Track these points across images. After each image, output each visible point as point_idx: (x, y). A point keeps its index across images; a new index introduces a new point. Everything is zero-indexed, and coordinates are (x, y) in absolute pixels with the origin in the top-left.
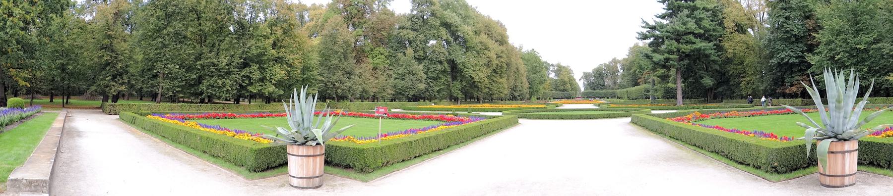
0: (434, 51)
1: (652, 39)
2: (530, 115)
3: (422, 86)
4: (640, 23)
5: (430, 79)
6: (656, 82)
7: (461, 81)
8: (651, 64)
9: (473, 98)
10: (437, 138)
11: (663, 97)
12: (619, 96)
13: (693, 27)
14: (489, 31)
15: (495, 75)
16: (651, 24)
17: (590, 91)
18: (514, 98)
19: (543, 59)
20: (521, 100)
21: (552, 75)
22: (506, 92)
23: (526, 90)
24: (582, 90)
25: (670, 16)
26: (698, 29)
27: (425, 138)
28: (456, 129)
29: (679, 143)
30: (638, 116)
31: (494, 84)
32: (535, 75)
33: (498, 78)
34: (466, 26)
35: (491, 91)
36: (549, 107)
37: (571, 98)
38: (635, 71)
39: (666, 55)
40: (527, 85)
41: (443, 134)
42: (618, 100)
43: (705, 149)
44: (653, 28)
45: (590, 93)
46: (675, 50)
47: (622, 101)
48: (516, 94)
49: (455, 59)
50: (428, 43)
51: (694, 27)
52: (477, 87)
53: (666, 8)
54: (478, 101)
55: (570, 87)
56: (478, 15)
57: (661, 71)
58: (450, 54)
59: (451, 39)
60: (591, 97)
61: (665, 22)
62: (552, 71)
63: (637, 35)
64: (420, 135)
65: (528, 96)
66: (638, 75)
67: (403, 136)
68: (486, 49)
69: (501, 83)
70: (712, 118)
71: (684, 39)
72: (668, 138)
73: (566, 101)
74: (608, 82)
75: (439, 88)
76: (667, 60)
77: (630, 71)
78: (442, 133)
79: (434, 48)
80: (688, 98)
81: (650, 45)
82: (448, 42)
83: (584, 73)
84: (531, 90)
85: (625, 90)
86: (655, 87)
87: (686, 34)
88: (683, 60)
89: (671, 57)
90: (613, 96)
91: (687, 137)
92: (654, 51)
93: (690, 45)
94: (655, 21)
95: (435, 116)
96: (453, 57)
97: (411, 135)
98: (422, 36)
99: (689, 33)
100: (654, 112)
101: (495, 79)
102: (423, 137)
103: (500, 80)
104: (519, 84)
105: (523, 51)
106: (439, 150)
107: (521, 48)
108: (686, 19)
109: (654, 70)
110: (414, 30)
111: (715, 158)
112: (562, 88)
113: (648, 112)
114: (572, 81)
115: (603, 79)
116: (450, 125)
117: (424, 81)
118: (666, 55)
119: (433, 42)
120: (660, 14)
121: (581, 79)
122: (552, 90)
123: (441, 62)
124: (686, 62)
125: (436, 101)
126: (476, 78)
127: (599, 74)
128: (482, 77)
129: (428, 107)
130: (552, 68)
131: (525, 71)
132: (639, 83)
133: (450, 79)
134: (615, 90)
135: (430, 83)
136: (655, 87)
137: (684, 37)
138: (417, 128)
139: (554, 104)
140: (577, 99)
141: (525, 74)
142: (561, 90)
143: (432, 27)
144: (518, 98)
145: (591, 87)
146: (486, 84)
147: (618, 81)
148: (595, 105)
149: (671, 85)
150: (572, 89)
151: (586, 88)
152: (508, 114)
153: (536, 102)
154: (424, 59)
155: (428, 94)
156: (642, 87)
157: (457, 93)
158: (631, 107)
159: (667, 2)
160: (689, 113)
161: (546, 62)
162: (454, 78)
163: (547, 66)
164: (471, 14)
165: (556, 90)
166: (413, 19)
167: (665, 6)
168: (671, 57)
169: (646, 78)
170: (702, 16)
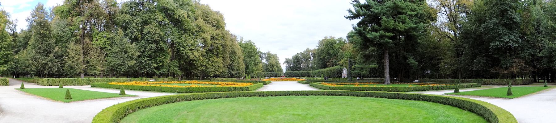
17: (291, 71)
31: (210, 63)
33: (215, 58)
35: (208, 69)
37: (277, 77)
38: (324, 57)
40: (244, 66)
45: (290, 73)
48: (234, 73)
55: (276, 69)
66: (327, 59)
69: (217, 62)
73: (274, 79)
83: (286, 59)
89: (387, 34)
101: (211, 59)
103: (216, 60)
112: (271, 69)
114: (277, 64)
115: (299, 63)
121: (284, 64)
122: (263, 71)
126: (192, 57)
127: (297, 60)
132: (328, 66)
134: (309, 71)
140: (282, 77)
141: (242, 58)
142: (270, 71)
144: (236, 76)
145: (291, 69)
150: (278, 70)
151: (288, 70)
163: (261, 54)
165: (267, 71)
168: (387, 34)
169: (333, 62)
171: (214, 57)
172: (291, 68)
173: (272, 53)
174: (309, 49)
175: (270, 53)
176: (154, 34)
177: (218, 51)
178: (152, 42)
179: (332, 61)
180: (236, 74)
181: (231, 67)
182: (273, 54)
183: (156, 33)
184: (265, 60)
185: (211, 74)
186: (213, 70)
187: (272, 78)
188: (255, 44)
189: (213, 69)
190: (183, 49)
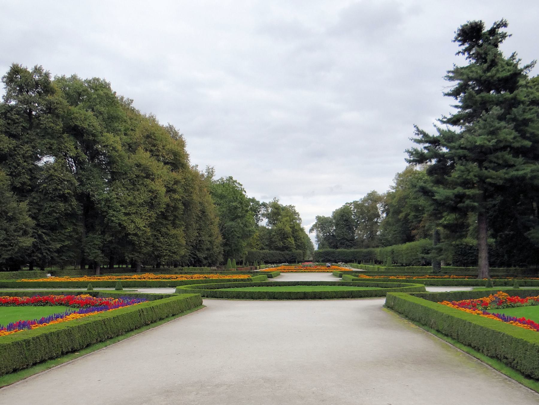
0: (50, 178)
1: (434, 162)
2: (223, 292)
3: (28, 242)
4: (411, 133)
5: (43, 227)
6: (442, 236)
7: (103, 233)
8: (431, 205)
9: (123, 262)
10: (69, 332)
11: (456, 262)
12: (379, 259)
13: (510, 138)
14: (154, 146)
15: (164, 222)
16: (431, 135)
18: (196, 262)
19: (249, 195)
20: (210, 265)
21: (264, 222)
22: (183, 252)
23: (218, 249)
24: (316, 247)
25: (468, 118)
26: (519, 139)
27: (51, 334)
28: (100, 319)
29: (446, 342)
30: (395, 297)
31: (162, 239)
32: (233, 223)
34: (110, 135)
35: (157, 250)
36: (256, 279)
37: (295, 262)
38: (407, 215)
39: (459, 190)
40: (220, 240)
41: (79, 327)
42: (376, 266)
43: (483, 352)
44: (435, 142)
46: (476, 180)
47: (382, 268)
48: (201, 255)
49: (91, 193)
50: (39, 160)
51: (512, 136)
52: (132, 243)
53: (460, 104)
54: (134, 269)
55: (293, 242)
56: (134, 114)
57: (449, 218)
58: (82, 183)
59: (85, 157)
60: (329, 261)
61: (457, 130)
62: (263, 215)
63: (407, 156)
64: (38, 330)
65: (221, 258)
67: (7, 333)
68: (148, 176)
69: (175, 236)
70: (532, 305)
71: (491, 162)
72: (434, 332)
73: (287, 268)
74: (359, 234)
75: (59, 245)
76: (460, 197)
77: (398, 215)
78: (77, 325)
79: (52, 171)
80: (501, 265)
81: (431, 171)
82: (79, 163)
83: (319, 218)
84: (228, 248)
85: (389, 248)
86: (439, 245)
87: (495, 149)
88: (491, 196)
89: (468, 192)
90: (369, 258)
91: (460, 332)
92: (438, 182)
93: (504, 170)
94: (439, 130)
95: (57, 297)
96: (88, 189)
97: (22, 330)
98: (26, 147)
99: (504, 148)
100: (430, 290)
101: (164, 230)
102: (47, 332)
103: (173, 232)
104: (205, 238)
105: (215, 178)
106: (74, 351)
107: (211, 173)
108: (497, 124)
109: (436, 215)
110: (11, 135)
111: (495, 366)
113: (419, 290)
116: (86, 312)
117: (31, 231)
118: (459, 190)
119: (48, 160)
120: (449, 117)
122: (262, 249)
123: (64, 198)
124: (499, 199)
125: (54, 269)
128: (141, 225)
129: (41, 280)
130: (263, 211)
131: (216, 217)
133: (81, 229)
135: (44, 236)
136: (439, 245)
137: (492, 157)
138: (31, 319)
139: (264, 273)
140: (306, 264)
142: (277, 249)
143: (46, 133)
144: (205, 262)
145: (330, 243)
146: (149, 239)
147: (378, 233)
148: (335, 275)
149: (470, 240)
151: (321, 246)
152: (186, 292)
153: (234, 270)
154: (31, 191)
155: (40, 255)
156: (420, 243)
157: (94, 255)
158: (394, 281)
159: (462, 94)
160: (487, 294)
161: (253, 200)
162: (90, 228)
164: (121, 112)
165: (271, 248)
166: (9, 115)
167: (457, 102)
168: (468, 192)
170: (528, 116)
171: (168, 226)
172: (331, 241)
173: (284, 202)
174: (376, 192)
175: (279, 203)
176: (61, 181)
177: (176, 213)
178: (55, 197)
179: (424, 227)
180: (206, 258)
181: (197, 246)
182: (284, 205)
183: (64, 180)
184: (267, 220)
185: (163, 259)
186: (167, 251)
187: (282, 266)
188: (242, 187)
189: (166, 250)
190: (114, 213)
